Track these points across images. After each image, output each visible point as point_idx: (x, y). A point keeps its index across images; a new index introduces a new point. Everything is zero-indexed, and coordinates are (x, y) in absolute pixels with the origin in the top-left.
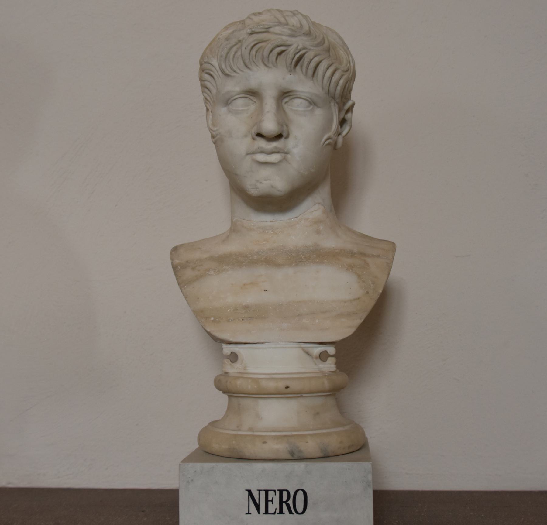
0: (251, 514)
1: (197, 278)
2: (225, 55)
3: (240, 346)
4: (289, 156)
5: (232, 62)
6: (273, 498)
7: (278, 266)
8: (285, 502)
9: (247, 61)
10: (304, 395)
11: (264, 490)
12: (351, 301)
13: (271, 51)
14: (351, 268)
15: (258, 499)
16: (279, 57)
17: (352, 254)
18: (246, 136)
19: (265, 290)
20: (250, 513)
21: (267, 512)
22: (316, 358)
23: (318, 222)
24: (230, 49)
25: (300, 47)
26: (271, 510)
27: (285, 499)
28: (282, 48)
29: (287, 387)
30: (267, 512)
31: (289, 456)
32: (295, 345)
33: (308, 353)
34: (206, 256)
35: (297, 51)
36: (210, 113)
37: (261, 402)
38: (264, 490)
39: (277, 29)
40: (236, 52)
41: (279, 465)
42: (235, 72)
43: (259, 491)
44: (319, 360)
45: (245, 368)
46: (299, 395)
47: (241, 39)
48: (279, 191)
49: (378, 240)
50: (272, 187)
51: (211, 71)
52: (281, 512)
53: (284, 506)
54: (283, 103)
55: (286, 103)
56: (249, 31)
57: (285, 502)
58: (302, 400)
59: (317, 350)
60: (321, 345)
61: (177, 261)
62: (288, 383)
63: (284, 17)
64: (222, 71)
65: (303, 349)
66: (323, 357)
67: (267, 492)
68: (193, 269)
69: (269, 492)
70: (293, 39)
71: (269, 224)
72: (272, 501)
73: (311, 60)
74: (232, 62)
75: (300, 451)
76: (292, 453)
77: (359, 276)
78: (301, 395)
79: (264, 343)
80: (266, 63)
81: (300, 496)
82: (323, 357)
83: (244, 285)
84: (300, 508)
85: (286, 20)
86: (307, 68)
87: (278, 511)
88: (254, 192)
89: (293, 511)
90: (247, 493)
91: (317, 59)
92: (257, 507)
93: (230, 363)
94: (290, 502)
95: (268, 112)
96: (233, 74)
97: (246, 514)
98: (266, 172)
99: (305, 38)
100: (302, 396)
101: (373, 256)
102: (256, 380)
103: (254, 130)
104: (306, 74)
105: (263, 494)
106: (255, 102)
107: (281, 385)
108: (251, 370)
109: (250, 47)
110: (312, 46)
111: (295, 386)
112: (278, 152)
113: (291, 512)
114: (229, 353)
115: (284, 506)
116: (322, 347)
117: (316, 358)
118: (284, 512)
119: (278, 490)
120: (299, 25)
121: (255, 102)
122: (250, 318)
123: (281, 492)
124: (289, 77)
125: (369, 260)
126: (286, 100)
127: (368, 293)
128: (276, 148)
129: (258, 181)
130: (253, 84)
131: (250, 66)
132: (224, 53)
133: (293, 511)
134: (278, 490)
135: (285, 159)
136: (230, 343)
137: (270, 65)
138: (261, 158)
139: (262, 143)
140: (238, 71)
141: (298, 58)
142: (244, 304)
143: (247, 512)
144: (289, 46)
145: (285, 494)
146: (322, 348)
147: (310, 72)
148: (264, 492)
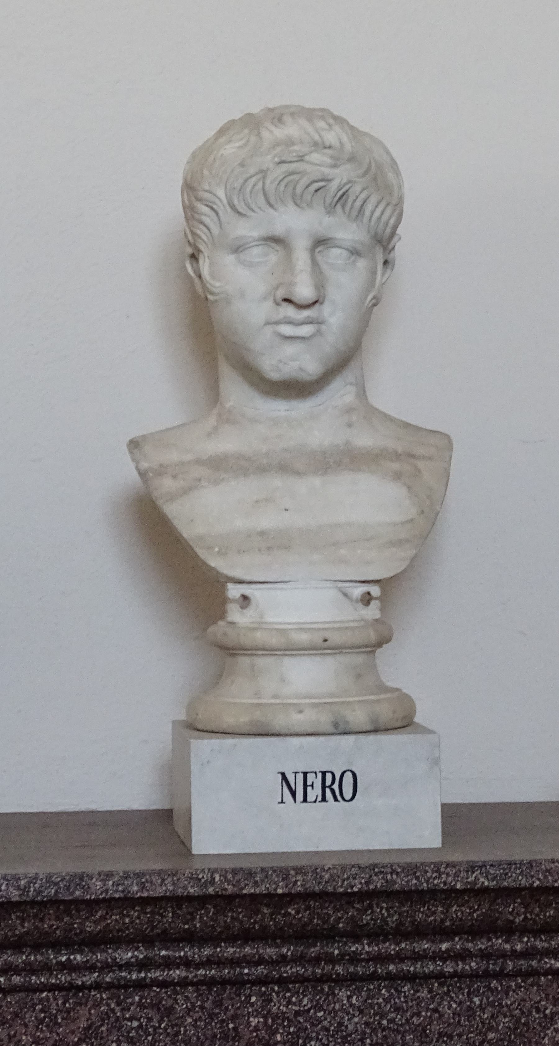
0: (284, 803)
1: (186, 491)
2: (239, 188)
3: (253, 586)
4: (323, 327)
5: (248, 196)
6: (313, 783)
7: (298, 474)
8: (330, 787)
9: (272, 199)
10: (344, 651)
11: (302, 772)
12: (403, 523)
13: (307, 187)
14: (397, 476)
15: (294, 784)
16: (315, 194)
17: (397, 456)
18: (265, 298)
19: (285, 510)
20: (284, 801)
21: (305, 800)
22: (357, 601)
23: (349, 410)
24: (246, 180)
25: (345, 180)
26: (310, 797)
27: (328, 782)
28: (321, 184)
29: (325, 640)
30: (305, 800)
31: (332, 729)
32: (328, 584)
33: (345, 595)
34: (189, 457)
35: (340, 187)
36: (207, 260)
37: (287, 661)
38: (302, 772)
39: (315, 157)
40: (254, 186)
41: (322, 739)
42: (253, 210)
43: (296, 773)
44: (360, 604)
45: (262, 617)
46: (338, 651)
47: (264, 168)
48: (310, 375)
49: (427, 430)
50: (301, 369)
51: (214, 203)
52: (324, 799)
53: (328, 792)
54: (316, 253)
55: (319, 252)
56: (277, 160)
57: (330, 787)
58: (340, 658)
59: (359, 590)
60: (363, 585)
61: (144, 465)
62: (327, 635)
63: (317, 131)
64: (233, 207)
65: (340, 589)
66: (367, 599)
67: (305, 774)
68: (175, 477)
69: (308, 775)
70: (336, 171)
71: (283, 413)
72: (312, 785)
73: (357, 197)
74: (248, 196)
75: (347, 722)
76: (336, 725)
77: (409, 488)
78: (340, 650)
79: (290, 582)
80: (298, 202)
81: (348, 779)
82: (367, 599)
83: (257, 502)
84: (348, 793)
85: (320, 136)
86: (352, 207)
87: (320, 798)
88: (274, 376)
89: (339, 798)
90: (280, 776)
91: (363, 196)
92: (293, 794)
93: (240, 609)
94: (336, 787)
95: (301, 271)
96: (250, 213)
97: (279, 803)
98: (290, 349)
99: (348, 166)
100: (341, 652)
101: (424, 458)
102: (283, 632)
103: (280, 294)
104: (349, 216)
105: (300, 777)
106: (277, 251)
107: (317, 639)
108: (269, 618)
109: (277, 183)
110: (358, 177)
111: (336, 638)
112: (311, 323)
113: (336, 799)
114: (238, 596)
115: (328, 792)
116: (363, 586)
117: (357, 601)
118: (327, 800)
119: (320, 772)
120: (338, 145)
121: (277, 251)
122: (269, 549)
123: (324, 774)
124: (327, 220)
125: (421, 464)
126: (320, 249)
127: (423, 512)
128: (308, 317)
129: (280, 361)
130: (279, 230)
131: (275, 206)
132: (237, 185)
133: (339, 798)
134: (320, 772)
135: (319, 332)
136: (241, 582)
137: (304, 205)
138: (287, 330)
139: (289, 311)
140: (256, 209)
141: (334, 192)
142: (259, 529)
143: (280, 800)
144: (330, 181)
145: (329, 777)
146: (364, 588)
147: (355, 213)
148: (302, 775)
